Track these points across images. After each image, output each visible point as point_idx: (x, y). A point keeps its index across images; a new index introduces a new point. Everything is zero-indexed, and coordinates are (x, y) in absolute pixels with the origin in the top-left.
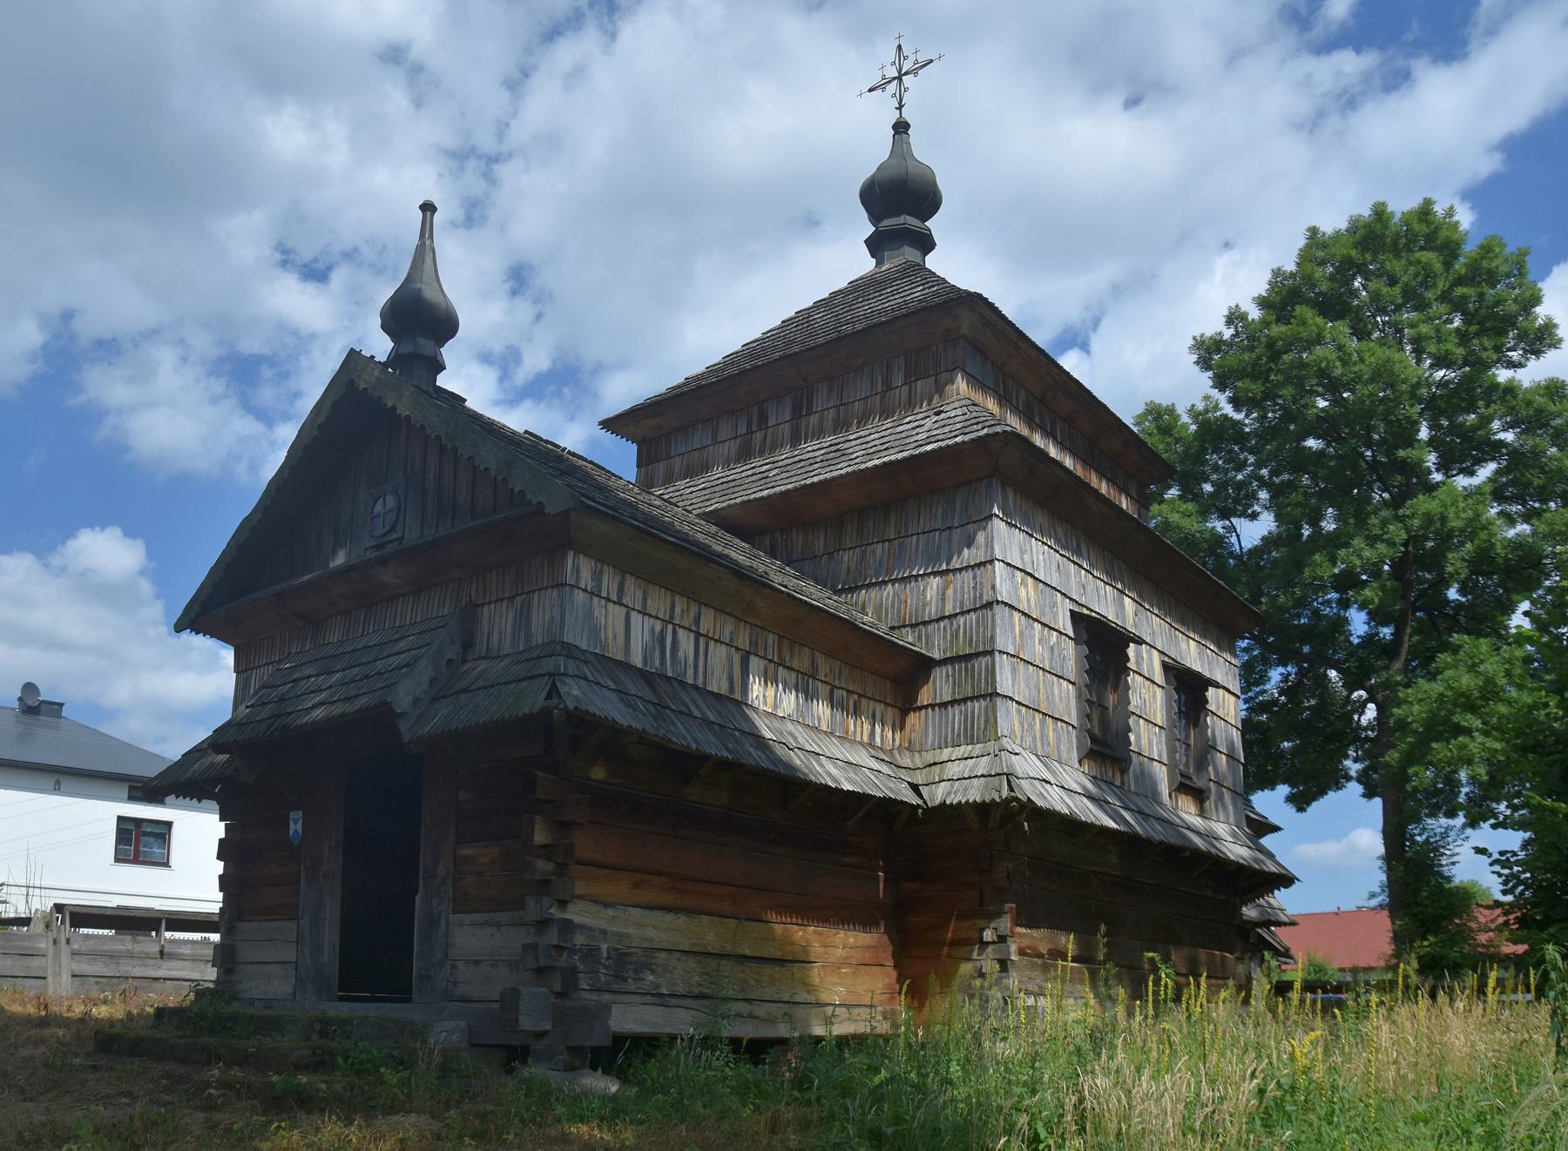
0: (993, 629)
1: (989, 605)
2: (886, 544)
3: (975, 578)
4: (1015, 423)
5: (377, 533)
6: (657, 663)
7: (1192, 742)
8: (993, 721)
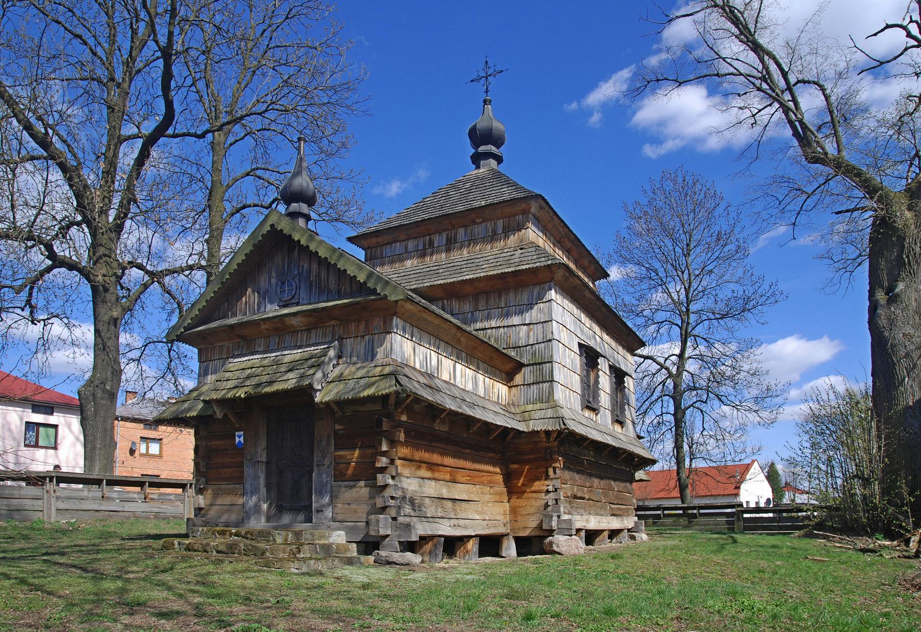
1: (550, 340)
4: (565, 260)
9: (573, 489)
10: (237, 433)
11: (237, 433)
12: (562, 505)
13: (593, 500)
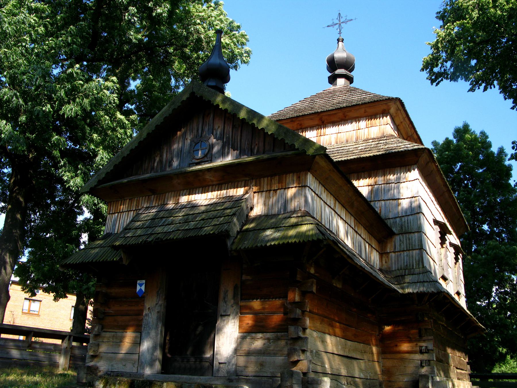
10: (138, 282)
11: (138, 282)
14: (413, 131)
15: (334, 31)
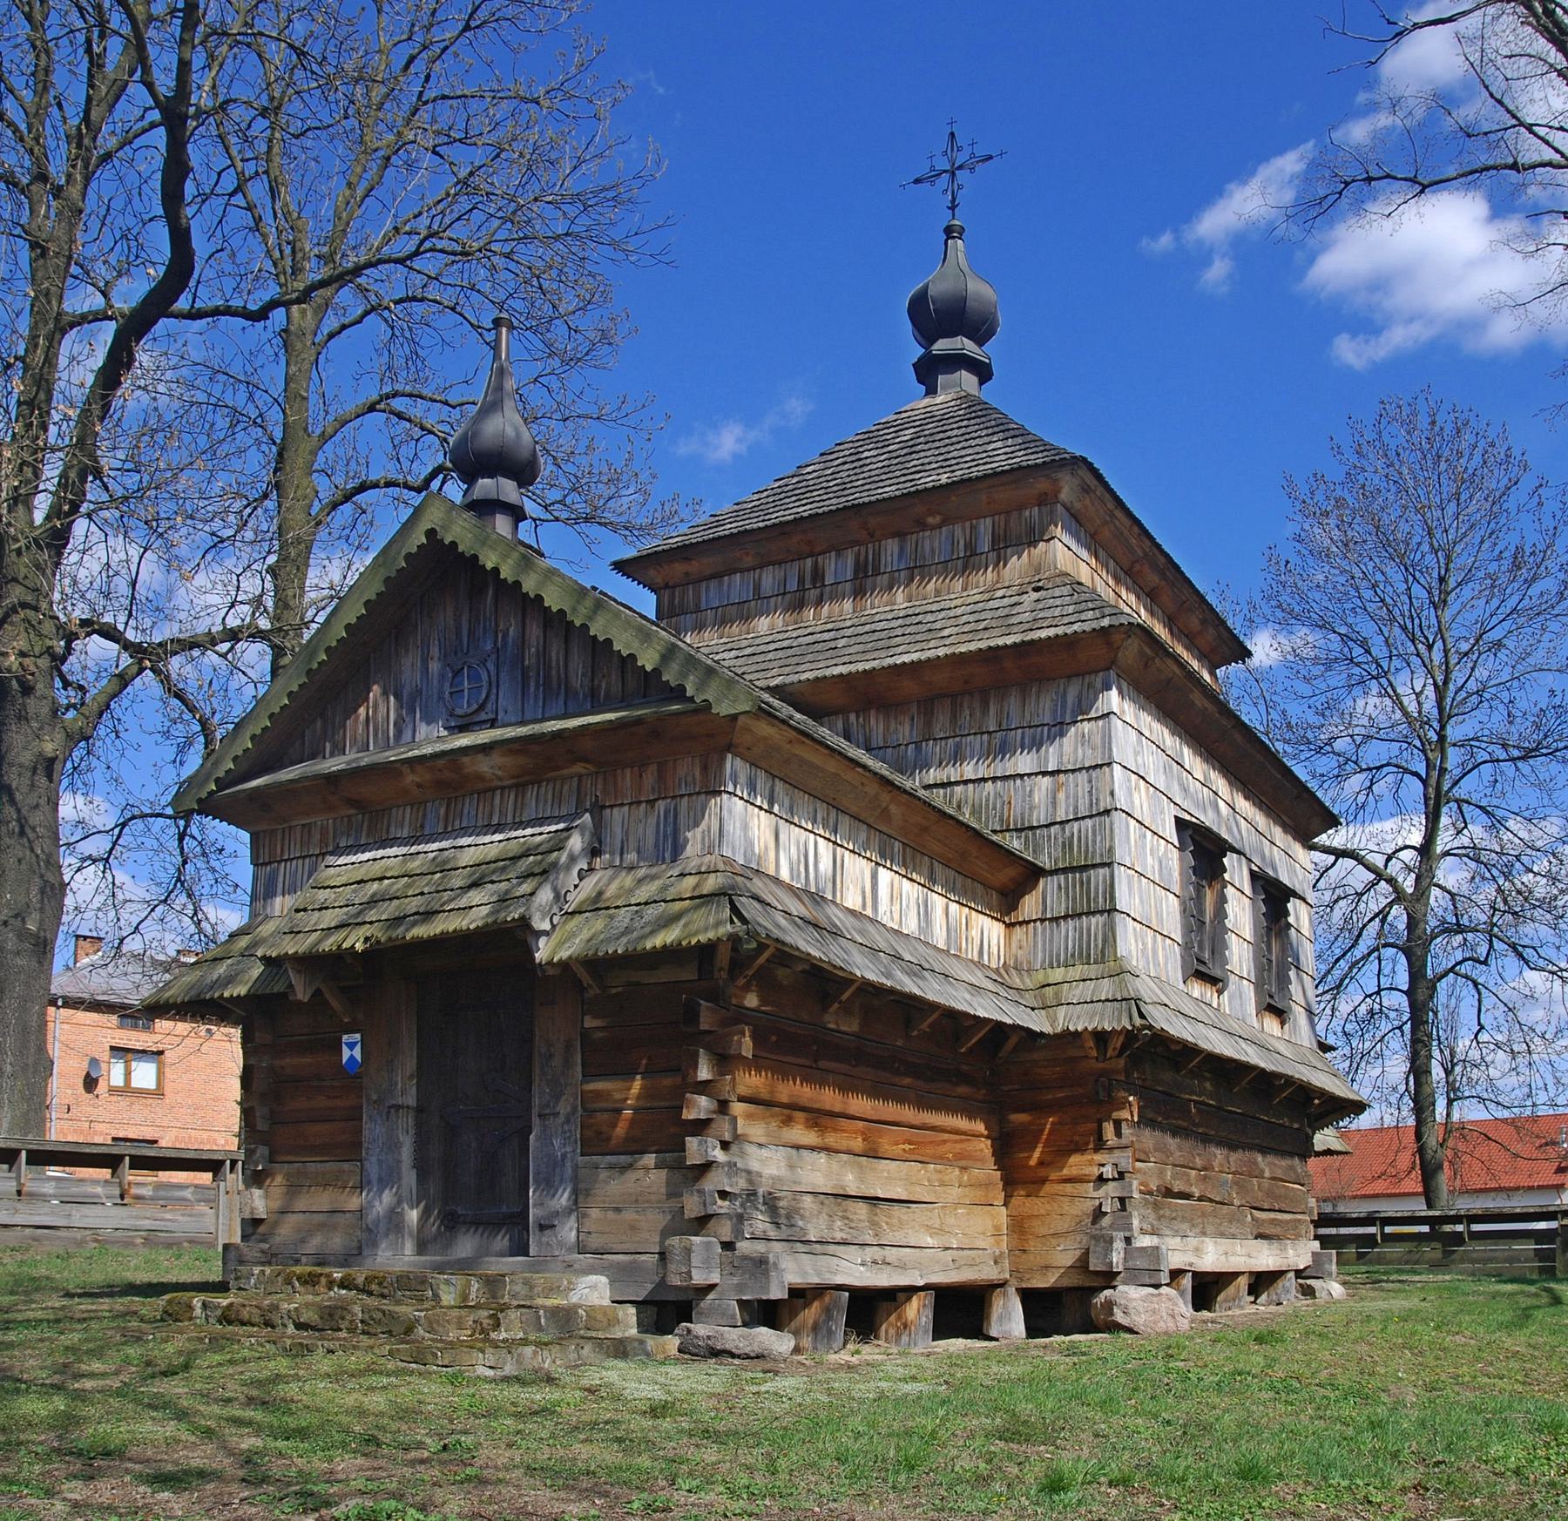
0: (1112, 839)
1: (1107, 812)
2: (985, 737)
3: (1090, 781)
5: (459, 711)
6: (803, 881)
7: (1274, 958)
8: (1111, 938)
9: (1161, 1173)
10: (345, 1037)
11: (345, 1037)
12: (1135, 1213)
13: (1211, 1200)
14: (1148, 543)
15: (936, 196)
